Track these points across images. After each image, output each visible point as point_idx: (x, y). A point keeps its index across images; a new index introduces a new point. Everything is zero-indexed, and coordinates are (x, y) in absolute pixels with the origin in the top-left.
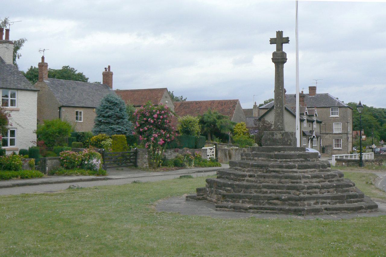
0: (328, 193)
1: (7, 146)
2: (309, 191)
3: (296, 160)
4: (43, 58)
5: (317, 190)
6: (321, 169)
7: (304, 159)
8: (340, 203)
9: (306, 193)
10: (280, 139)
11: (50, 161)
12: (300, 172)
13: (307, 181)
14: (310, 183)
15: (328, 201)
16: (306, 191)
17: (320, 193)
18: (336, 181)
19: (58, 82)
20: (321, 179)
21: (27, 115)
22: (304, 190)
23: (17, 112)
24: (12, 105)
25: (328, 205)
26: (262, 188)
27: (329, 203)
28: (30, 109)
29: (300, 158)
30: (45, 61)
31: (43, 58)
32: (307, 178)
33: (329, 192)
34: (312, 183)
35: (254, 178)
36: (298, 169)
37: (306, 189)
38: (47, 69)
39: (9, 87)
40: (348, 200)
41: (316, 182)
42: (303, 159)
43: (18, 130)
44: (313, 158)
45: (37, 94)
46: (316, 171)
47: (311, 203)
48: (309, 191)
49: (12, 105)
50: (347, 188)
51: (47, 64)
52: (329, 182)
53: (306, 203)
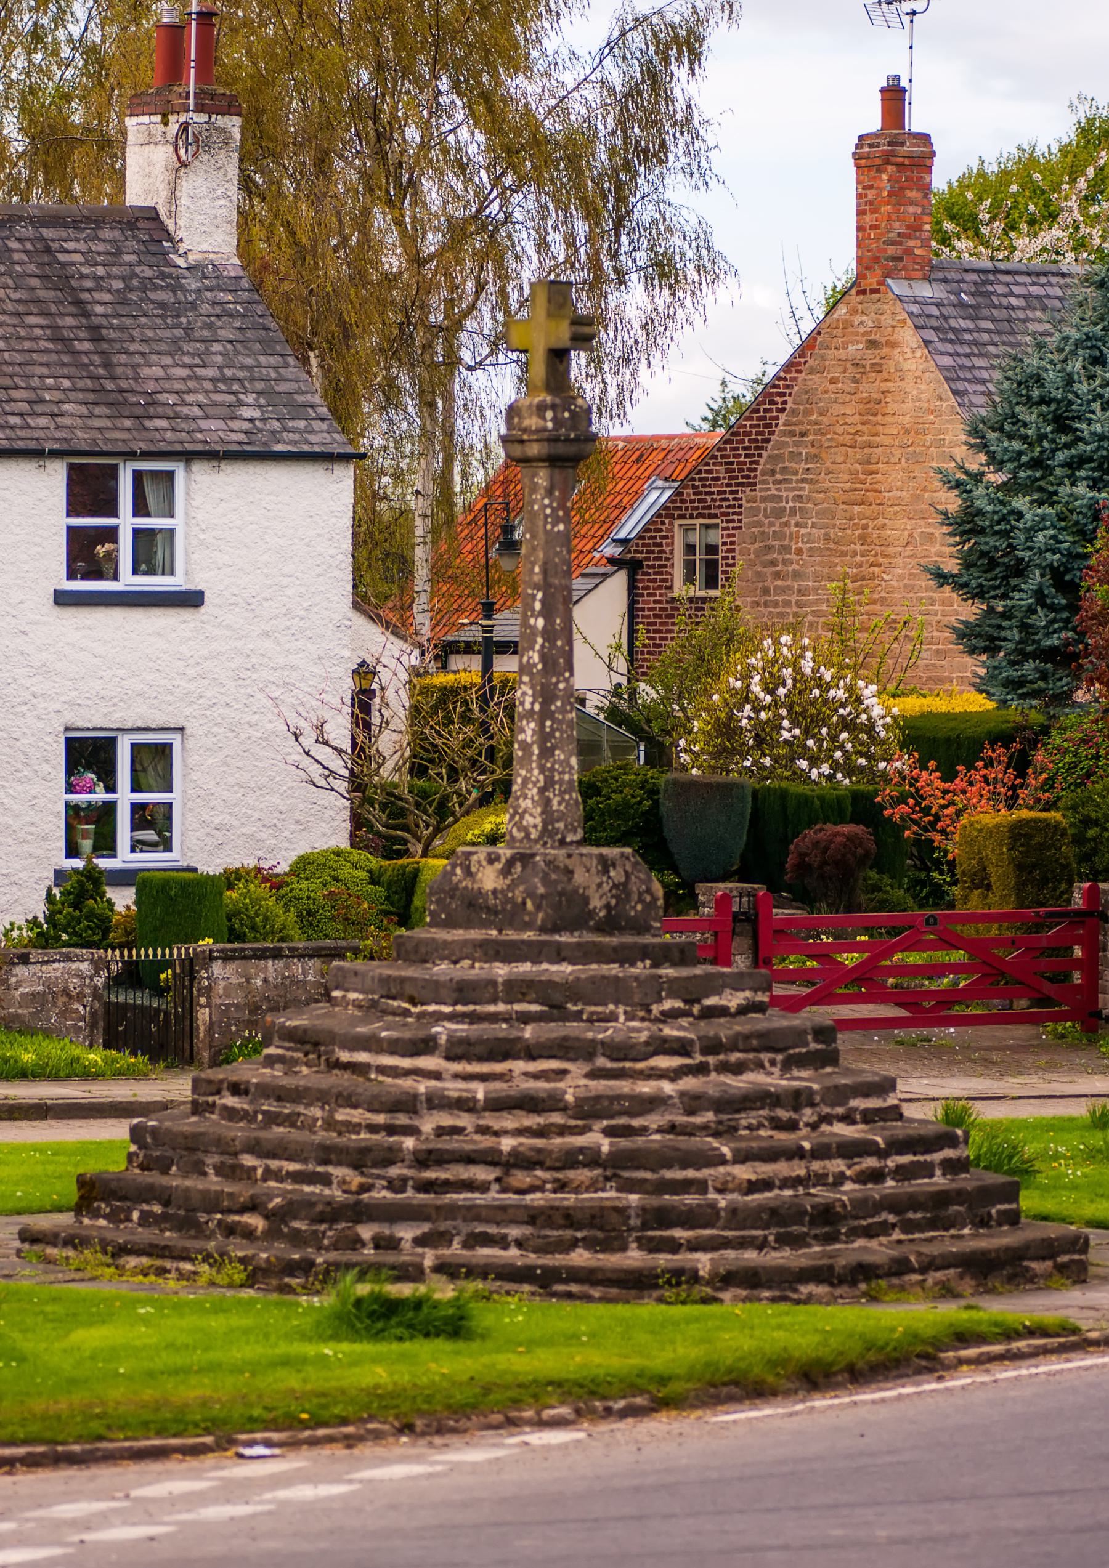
0: (555, 1191)
1: (115, 856)
2: (430, 1174)
3: (492, 1008)
4: (894, 96)
5: (482, 1173)
6: (602, 1062)
7: (542, 1004)
8: (590, 1244)
9: (411, 1183)
10: (494, 892)
11: (232, 966)
12: (456, 1076)
13: (460, 1123)
14: (478, 1137)
15: (514, 1232)
16: (406, 1172)
17: (504, 1190)
18: (659, 1131)
19: (1035, 290)
20: (557, 1118)
21: (267, 634)
22: (394, 1171)
23: (186, 614)
24: (144, 563)
25: (513, 1252)
26: (243, 1151)
27: (519, 1244)
28: (289, 592)
29: (520, 1001)
30: (917, 120)
31: (894, 96)
32: (460, 1109)
33: (561, 1186)
34: (497, 1134)
35: (244, 1099)
36: (448, 1058)
37: (407, 1163)
38: (926, 189)
39: (144, 446)
40: (650, 1233)
41: (520, 1132)
42: (535, 1008)
43: (190, 743)
44: (606, 1005)
45: (350, 482)
46: (565, 1072)
47: (401, 1234)
48: (430, 1174)
49: (144, 563)
50: (690, 1173)
51: (925, 138)
52: (608, 1132)
53: (366, 1232)
